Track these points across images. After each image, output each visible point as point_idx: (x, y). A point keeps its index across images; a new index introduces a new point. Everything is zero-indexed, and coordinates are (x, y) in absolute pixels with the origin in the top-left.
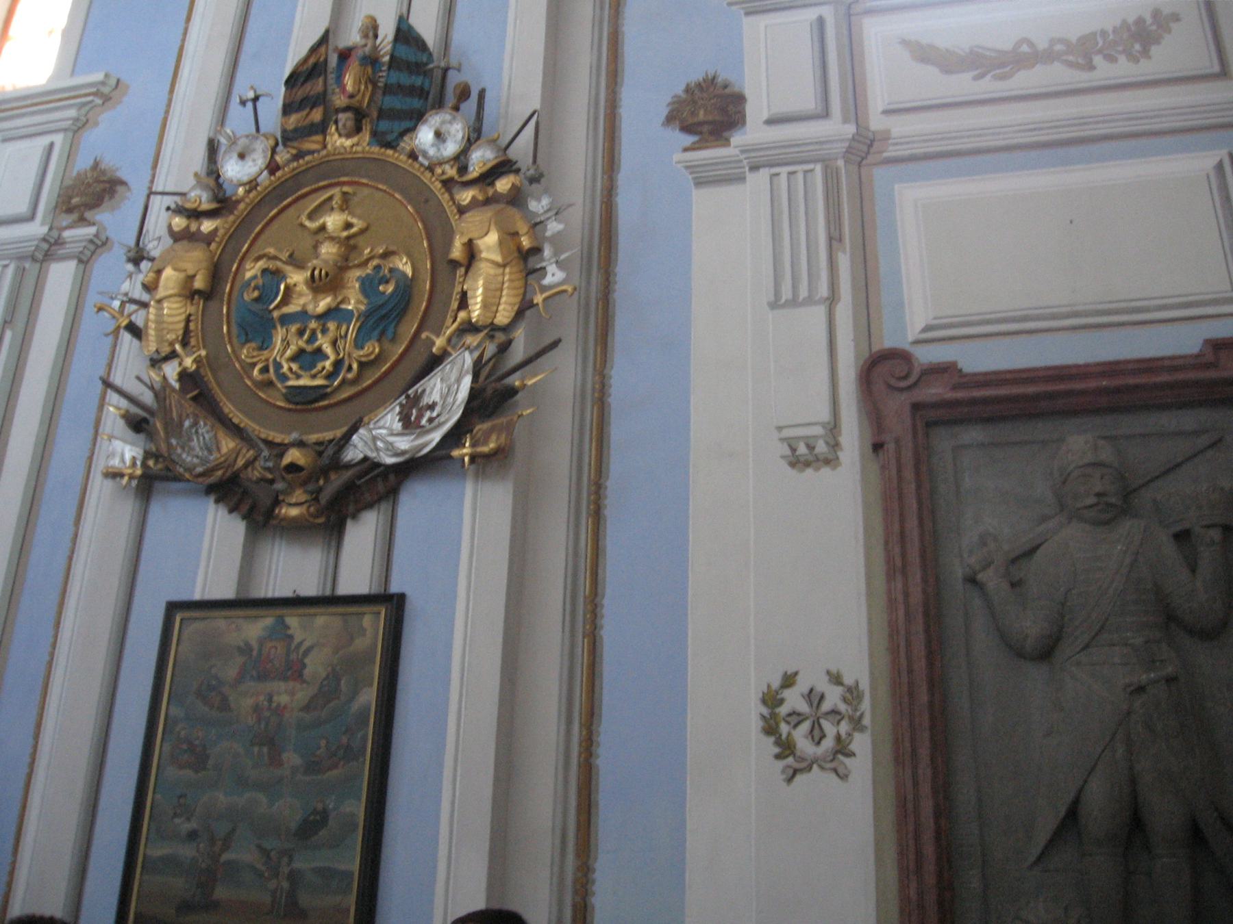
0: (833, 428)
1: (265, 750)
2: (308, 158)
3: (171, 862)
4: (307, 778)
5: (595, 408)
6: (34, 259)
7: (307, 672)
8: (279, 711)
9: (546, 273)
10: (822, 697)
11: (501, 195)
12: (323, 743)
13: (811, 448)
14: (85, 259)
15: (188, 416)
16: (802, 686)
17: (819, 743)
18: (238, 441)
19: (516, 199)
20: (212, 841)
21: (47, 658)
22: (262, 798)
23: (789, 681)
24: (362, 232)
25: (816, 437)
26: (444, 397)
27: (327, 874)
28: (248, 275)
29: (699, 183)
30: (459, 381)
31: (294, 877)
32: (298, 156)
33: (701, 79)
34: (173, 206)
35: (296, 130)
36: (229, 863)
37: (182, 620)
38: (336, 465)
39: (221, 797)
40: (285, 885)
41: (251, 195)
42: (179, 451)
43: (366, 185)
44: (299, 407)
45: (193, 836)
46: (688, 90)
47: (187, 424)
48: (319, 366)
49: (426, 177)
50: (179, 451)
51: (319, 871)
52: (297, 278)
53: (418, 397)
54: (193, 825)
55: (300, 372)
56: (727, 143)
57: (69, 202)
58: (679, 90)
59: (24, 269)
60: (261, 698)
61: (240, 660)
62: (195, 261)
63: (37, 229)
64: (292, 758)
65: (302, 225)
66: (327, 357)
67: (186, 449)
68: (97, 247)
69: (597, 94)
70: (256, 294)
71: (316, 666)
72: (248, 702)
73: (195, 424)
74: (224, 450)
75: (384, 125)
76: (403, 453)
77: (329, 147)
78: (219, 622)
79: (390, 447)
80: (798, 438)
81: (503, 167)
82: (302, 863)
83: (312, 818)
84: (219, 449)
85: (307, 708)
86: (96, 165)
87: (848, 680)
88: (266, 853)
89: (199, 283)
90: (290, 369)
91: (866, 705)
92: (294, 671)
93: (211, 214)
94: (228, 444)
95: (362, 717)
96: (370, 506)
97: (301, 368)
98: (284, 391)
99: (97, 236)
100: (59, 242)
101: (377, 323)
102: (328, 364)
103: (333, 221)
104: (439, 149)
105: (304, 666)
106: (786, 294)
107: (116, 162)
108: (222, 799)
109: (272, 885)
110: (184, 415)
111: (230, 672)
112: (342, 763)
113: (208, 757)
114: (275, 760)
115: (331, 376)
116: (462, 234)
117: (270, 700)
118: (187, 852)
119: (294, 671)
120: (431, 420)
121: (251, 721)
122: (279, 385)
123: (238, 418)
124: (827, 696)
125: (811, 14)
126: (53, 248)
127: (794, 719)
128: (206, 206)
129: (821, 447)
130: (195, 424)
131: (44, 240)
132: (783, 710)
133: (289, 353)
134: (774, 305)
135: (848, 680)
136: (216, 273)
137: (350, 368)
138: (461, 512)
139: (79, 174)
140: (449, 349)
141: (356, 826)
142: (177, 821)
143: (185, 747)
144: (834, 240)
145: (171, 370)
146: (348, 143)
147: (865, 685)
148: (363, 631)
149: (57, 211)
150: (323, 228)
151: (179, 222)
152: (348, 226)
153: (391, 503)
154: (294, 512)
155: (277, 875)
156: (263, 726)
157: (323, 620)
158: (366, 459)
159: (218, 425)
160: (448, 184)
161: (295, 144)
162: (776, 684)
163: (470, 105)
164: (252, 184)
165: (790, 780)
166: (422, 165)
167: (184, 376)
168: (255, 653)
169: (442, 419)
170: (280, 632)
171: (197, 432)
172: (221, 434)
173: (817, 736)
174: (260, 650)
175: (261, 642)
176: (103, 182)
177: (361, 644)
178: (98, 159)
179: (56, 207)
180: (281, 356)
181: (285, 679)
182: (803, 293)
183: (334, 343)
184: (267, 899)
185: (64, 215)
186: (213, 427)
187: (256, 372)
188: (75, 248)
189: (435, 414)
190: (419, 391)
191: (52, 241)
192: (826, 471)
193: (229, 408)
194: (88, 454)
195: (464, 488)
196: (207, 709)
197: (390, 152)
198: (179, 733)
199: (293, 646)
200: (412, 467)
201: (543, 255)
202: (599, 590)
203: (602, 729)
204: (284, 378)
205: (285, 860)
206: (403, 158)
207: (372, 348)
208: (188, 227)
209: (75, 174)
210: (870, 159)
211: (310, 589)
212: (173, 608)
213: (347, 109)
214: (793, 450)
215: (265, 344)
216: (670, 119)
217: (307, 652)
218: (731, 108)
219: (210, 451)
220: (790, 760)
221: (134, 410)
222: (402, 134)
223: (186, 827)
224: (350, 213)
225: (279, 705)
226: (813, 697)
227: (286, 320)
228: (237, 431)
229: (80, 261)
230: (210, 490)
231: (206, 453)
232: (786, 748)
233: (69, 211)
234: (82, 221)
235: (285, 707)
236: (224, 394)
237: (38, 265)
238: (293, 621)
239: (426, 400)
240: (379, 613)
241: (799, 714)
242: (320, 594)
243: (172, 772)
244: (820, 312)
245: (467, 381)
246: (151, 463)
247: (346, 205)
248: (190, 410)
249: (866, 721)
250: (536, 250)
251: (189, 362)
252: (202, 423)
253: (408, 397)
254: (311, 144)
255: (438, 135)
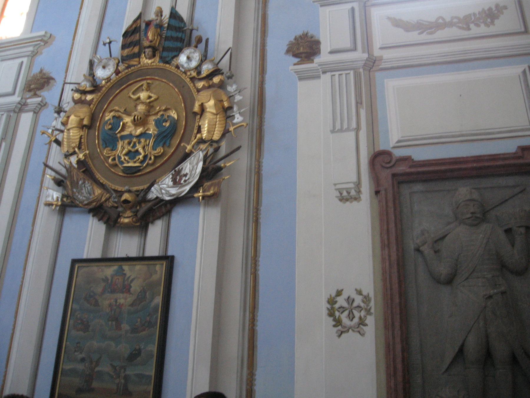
0: (358, 184)
1: (114, 323)
2: (132, 68)
3: (73, 371)
4: (132, 335)
5: (256, 176)
6: (15, 112)
7: (132, 289)
8: (120, 306)
9: (235, 118)
10: (353, 300)
11: (215, 84)
12: (139, 320)
13: (348, 193)
14: (37, 111)
15: (81, 179)
16: (345, 295)
17: (352, 320)
18: (102, 190)
19: (222, 86)
20: (91, 362)
21: (20, 283)
22: (113, 344)
23: (339, 293)
24: (156, 100)
25: (351, 188)
26: (191, 171)
27: (140, 376)
28: (107, 118)
29: (301, 79)
30: (197, 164)
31: (126, 378)
32: (128, 67)
33: (301, 34)
34: (74, 89)
35: (127, 56)
36: (98, 372)
37: (78, 267)
38: (144, 200)
39: (95, 343)
40: (123, 381)
41: (108, 84)
42: (77, 194)
43: (157, 80)
44: (128, 175)
45: (83, 360)
46: (296, 39)
47: (80, 182)
48: (137, 158)
49: (183, 76)
50: (77, 194)
51: (137, 375)
52: (128, 120)
53: (180, 171)
54: (83, 355)
55: (129, 160)
56: (312, 62)
57: (30, 87)
58: (292, 39)
59: (10, 116)
60: (112, 301)
61: (103, 284)
62: (84, 112)
63: (16, 98)
64: (125, 327)
65: (130, 97)
66: (141, 154)
67: (80, 193)
68: (42, 106)
69: (257, 41)
70: (110, 127)
71: (136, 287)
72: (107, 302)
73: (84, 183)
74: (96, 194)
75: (165, 54)
76: (173, 195)
77: (142, 63)
78: (94, 268)
79: (168, 193)
80: (343, 189)
81: (216, 72)
82: (130, 372)
83: (134, 352)
84: (94, 194)
85: (132, 305)
86: (41, 71)
87: (365, 293)
88: (114, 367)
89: (85, 122)
90: (125, 159)
91: (372, 304)
92: (126, 289)
93: (91, 92)
94: (98, 191)
95: (156, 309)
96: (159, 218)
97: (129, 158)
98: (122, 168)
99: (41, 101)
100: (25, 104)
101: (162, 139)
102: (141, 157)
103: (143, 95)
104: (189, 64)
105: (131, 287)
106: (338, 127)
107: (50, 70)
108: (95, 344)
109: (117, 381)
110: (79, 179)
111: (99, 289)
112: (147, 329)
113: (89, 326)
114: (118, 327)
115: (142, 162)
116: (199, 101)
117: (116, 302)
118: (80, 367)
119: (126, 289)
120: (185, 181)
121: (108, 310)
122: (120, 166)
123: (102, 180)
124: (356, 300)
125: (349, 6)
126: (23, 107)
127: (341, 310)
128: (88, 89)
129: (353, 193)
130: (84, 183)
131: (19, 103)
132: (337, 306)
133: (124, 152)
134: (333, 131)
135: (365, 293)
136: (93, 118)
137: (150, 159)
138: (198, 221)
139: (34, 75)
140: (193, 150)
141: (153, 356)
142: (76, 353)
143: (79, 322)
144: (359, 103)
145: (74, 160)
146: (150, 61)
147: (372, 295)
148: (156, 272)
149: (25, 91)
150: (139, 98)
151: (77, 96)
152: (150, 97)
153: (168, 217)
154: (126, 220)
155: (119, 377)
156: (113, 313)
157: (139, 267)
158: (157, 198)
159: (94, 183)
160: (192, 79)
161: (127, 62)
162: (333, 295)
163: (202, 45)
164: (108, 79)
165: (339, 336)
166: (181, 71)
167: (79, 162)
168: (109, 281)
169: (190, 180)
170: (121, 272)
171: (85, 186)
172: (95, 187)
173: (351, 317)
174: (112, 280)
175: (112, 276)
176: (44, 78)
177: (155, 277)
178: (42, 68)
179: (24, 89)
180: (121, 154)
181: (122, 292)
182: (345, 126)
183: (144, 148)
184: (115, 387)
185: (27, 93)
186: (91, 184)
187: (110, 160)
188: (32, 107)
189: (187, 178)
190: (180, 168)
191: (22, 104)
192: (355, 203)
193: (98, 176)
194: (38, 196)
195: (200, 210)
196: (89, 305)
197: (168, 65)
198: (77, 316)
199: (126, 278)
200: (177, 201)
201: (233, 110)
202: (258, 254)
203: (259, 314)
204: (122, 163)
205: (123, 370)
206: (173, 68)
207: (160, 150)
208: (81, 98)
209: (32, 75)
210: (374, 69)
211: (133, 254)
212: (74, 262)
213: (149, 47)
214: (341, 194)
215: (114, 148)
216: (288, 51)
217: (132, 281)
218: (314, 47)
219: (90, 194)
220: (340, 327)
221: (58, 177)
222: (173, 58)
223: (80, 356)
224: (150, 92)
225: (120, 304)
226: (350, 300)
227: (123, 138)
228: (102, 186)
229: (35, 112)
230: (90, 211)
231: (88, 195)
232: (338, 322)
233: (30, 91)
234: (35, 95)
235: (123, 305)
236: (96, 170)
237: (16, 114)
238: (126, 267)
239: (183, 172)
240: (163, 264)
241: (343, 308)
242: (138, 256)
243: (74, 333)
244: (352, 134)
245: (201, 164)
246: (65, 199)
247: (149, 88)
248: (82, 177)
249: (372, 311)
250: (230, 108)
251: (81, 156)
252: (87, 182)
253: (175, 171)
254: (134, 62)
255: (188, 58)
